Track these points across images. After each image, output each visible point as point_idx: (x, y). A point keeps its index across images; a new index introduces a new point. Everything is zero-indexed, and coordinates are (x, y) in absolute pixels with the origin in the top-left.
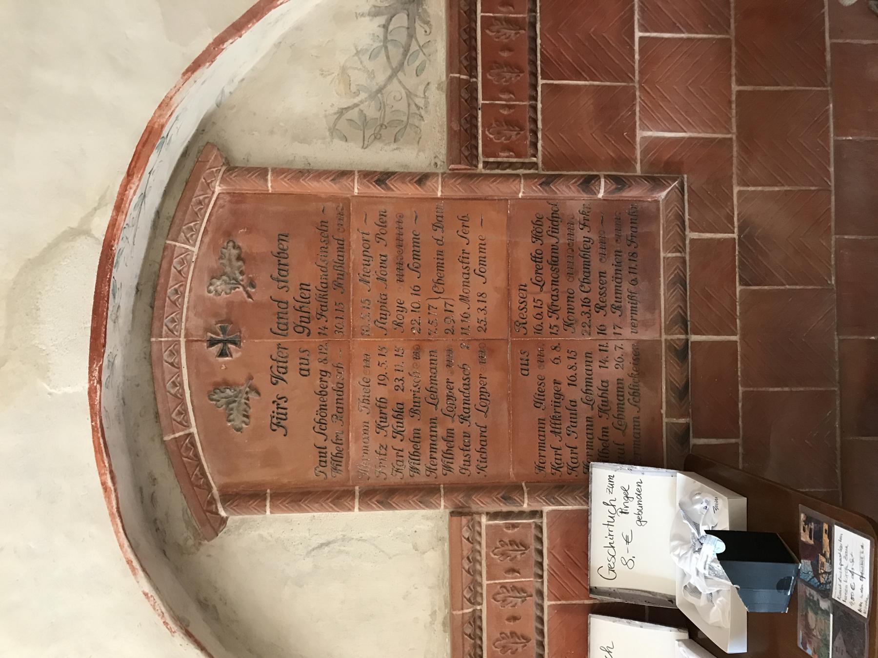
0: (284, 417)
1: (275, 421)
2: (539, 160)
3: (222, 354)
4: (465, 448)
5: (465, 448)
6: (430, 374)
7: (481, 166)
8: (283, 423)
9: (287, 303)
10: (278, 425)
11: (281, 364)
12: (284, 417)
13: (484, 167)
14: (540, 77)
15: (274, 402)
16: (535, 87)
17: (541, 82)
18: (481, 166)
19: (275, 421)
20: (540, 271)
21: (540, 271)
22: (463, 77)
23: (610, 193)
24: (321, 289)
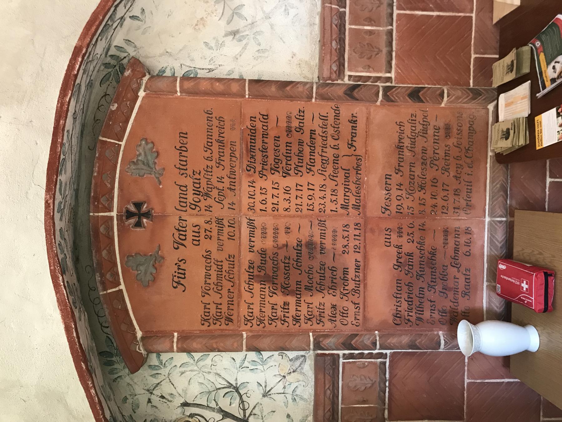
0: (183, 276)
1: (176, 279)
2: (392, 75)
3: (139, 224)
4: (324, 126)
5: (324, 126)
6: (335, 114)
7: (346, 78)
8: (182, 281)
9: (186, 187)
10: (178, 283)
11: (181, 233)
12: (183, 276)
13: (349, 80)
14: (395, 8)
15: (176, 264)
16: (391, 14)
17: (396, 12)
18: (346, 78)
19: (176, 279)
20: (221, 135)
21: (221, 135)
22: (333, 6)
23: (451, 102)
24: (411, 137)
